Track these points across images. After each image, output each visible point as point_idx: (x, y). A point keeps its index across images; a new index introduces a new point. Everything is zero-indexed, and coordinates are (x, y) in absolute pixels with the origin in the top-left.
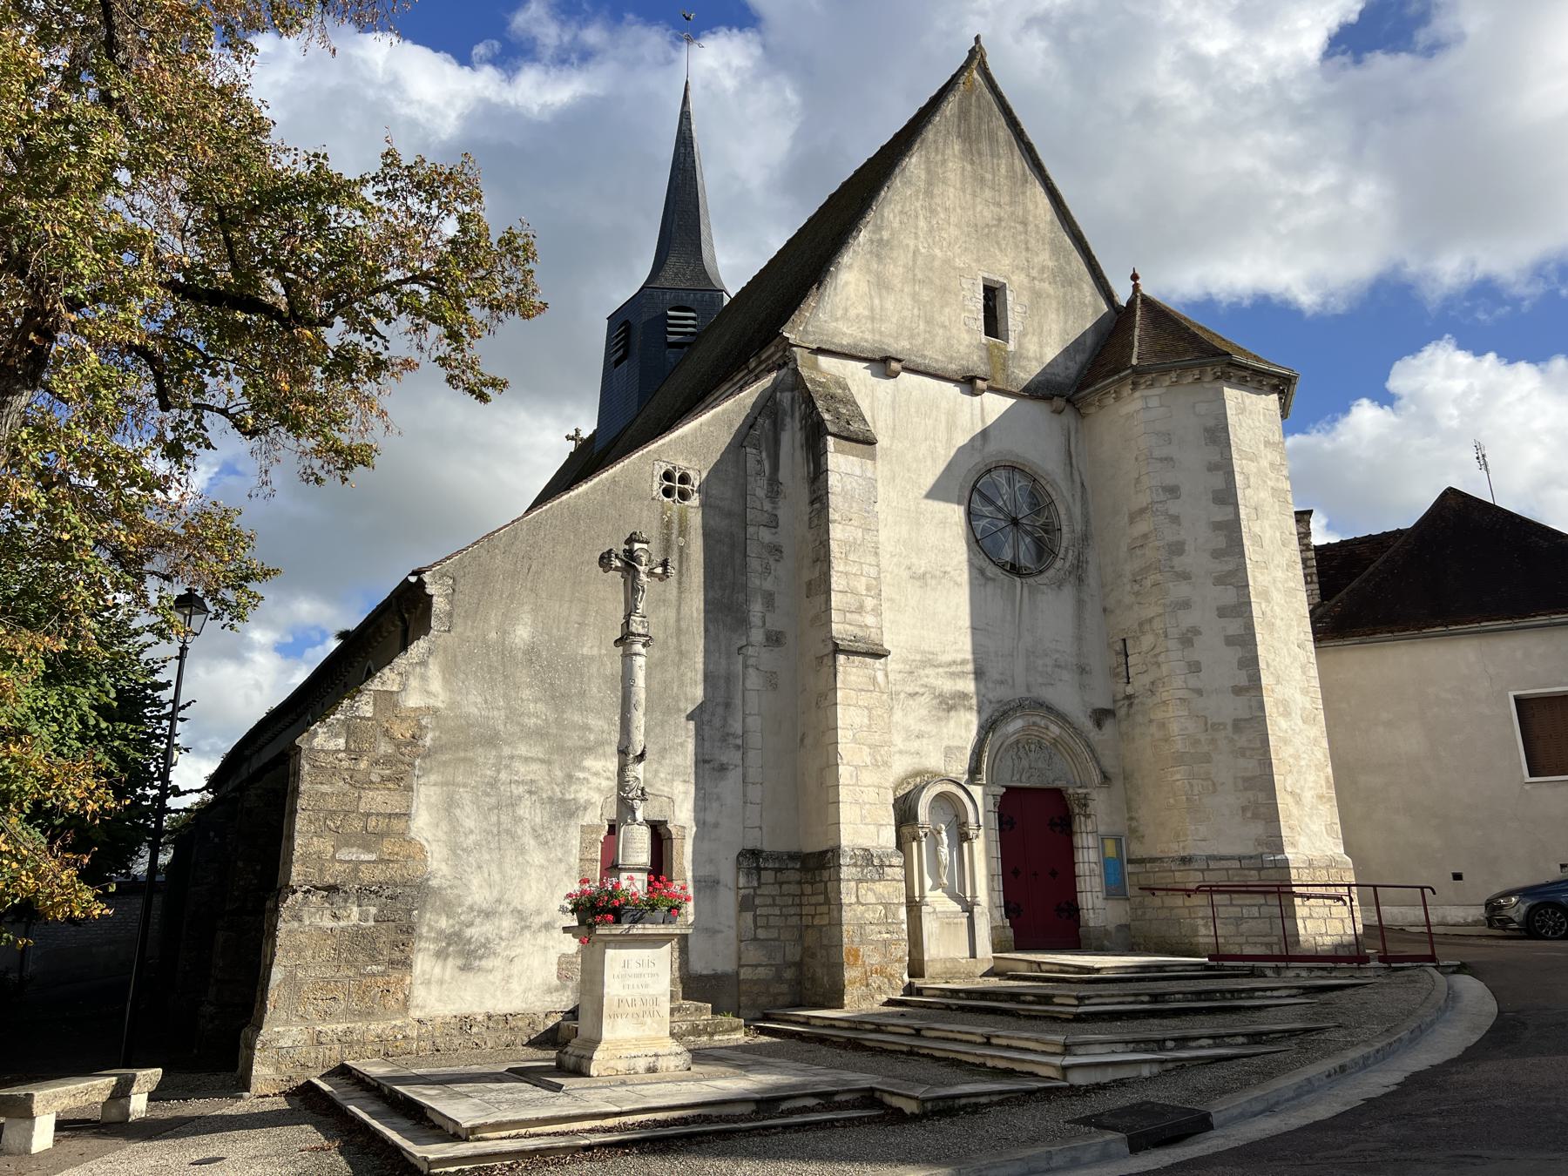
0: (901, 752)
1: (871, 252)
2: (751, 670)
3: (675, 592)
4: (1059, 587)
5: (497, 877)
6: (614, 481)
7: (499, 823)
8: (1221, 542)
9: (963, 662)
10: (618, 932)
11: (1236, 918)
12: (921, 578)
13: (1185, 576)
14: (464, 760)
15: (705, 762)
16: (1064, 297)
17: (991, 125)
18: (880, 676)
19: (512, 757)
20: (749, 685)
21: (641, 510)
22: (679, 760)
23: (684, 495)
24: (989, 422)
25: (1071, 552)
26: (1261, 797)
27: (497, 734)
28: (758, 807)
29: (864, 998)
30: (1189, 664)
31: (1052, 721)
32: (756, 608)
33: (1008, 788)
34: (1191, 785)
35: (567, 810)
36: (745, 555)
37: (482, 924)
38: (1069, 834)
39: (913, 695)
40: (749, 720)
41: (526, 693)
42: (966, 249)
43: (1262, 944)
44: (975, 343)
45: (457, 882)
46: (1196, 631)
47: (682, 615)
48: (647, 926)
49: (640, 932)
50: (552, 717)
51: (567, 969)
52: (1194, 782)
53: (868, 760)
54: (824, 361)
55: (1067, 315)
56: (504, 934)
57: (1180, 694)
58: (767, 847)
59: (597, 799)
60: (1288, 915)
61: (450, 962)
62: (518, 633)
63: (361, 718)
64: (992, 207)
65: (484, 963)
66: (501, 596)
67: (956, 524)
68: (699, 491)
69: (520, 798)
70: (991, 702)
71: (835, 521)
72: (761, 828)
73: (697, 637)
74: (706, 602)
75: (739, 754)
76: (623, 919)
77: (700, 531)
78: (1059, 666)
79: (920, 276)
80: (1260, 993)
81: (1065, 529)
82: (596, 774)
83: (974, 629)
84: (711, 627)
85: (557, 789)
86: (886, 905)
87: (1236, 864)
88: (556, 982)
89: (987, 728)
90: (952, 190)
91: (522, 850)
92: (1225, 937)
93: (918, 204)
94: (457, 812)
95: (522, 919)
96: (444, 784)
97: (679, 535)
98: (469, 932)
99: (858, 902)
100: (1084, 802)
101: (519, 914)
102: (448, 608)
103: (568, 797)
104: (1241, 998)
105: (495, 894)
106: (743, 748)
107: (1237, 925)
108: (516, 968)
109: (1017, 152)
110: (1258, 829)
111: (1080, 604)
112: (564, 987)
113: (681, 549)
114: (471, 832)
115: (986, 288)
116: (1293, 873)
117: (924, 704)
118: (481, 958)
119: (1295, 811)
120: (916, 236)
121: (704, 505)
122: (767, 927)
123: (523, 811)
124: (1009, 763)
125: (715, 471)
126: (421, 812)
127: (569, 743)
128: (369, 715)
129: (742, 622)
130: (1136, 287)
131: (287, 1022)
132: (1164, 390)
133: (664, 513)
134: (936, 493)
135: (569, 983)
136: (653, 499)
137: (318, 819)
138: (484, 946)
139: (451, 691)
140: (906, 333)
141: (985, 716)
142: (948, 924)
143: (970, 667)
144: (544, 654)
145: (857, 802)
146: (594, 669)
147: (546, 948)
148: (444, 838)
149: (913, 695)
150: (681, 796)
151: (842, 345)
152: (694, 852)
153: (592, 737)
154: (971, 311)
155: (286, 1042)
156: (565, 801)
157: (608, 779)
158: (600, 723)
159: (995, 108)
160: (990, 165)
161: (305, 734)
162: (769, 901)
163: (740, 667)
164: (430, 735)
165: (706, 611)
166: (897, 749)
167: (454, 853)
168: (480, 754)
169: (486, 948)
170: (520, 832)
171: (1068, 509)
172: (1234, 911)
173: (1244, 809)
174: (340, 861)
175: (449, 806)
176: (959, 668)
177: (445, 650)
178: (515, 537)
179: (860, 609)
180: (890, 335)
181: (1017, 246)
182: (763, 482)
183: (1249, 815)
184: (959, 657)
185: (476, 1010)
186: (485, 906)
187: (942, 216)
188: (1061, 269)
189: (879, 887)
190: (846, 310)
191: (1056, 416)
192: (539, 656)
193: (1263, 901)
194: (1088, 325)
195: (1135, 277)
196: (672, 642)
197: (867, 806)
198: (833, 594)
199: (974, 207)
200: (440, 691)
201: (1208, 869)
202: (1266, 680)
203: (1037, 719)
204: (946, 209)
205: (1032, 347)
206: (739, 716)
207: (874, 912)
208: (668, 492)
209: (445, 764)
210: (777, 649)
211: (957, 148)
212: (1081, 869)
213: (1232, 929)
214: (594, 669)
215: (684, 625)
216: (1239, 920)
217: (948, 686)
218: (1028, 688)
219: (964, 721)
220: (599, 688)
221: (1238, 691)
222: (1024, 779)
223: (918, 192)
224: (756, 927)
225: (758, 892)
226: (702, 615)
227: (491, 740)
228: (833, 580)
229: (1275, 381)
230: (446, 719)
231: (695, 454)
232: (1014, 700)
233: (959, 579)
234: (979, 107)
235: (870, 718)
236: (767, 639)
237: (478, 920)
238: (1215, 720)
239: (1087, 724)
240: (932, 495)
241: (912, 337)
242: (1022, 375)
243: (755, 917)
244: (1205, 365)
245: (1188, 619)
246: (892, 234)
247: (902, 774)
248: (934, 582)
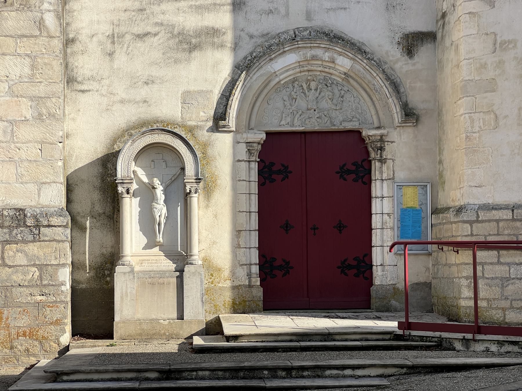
0: (122, 102)
11: (502, 279)
31: (340, 54)
33: (268, 134)
34: (472, 121)
39: (142, 37)
52: (476, 116)
53: (28, 114)
70: (251, 37)
80: (335, 372)
86: (41, 267)
87: (507, 215)
92: (488, 300)
104: (303, 377)
107: (503, 287)
124: (280, 104)
145: (11, 160)
149: (142, 37)
189: (33, 249)
197: (26, 164)
201: (477, 221)
203: (319, 52)
207: (25, 274)
212: (376, 221)
213: (496, 291)
216: (505, 281)
232: (286, 32)
235: (33, 67)
238: (506, 37)
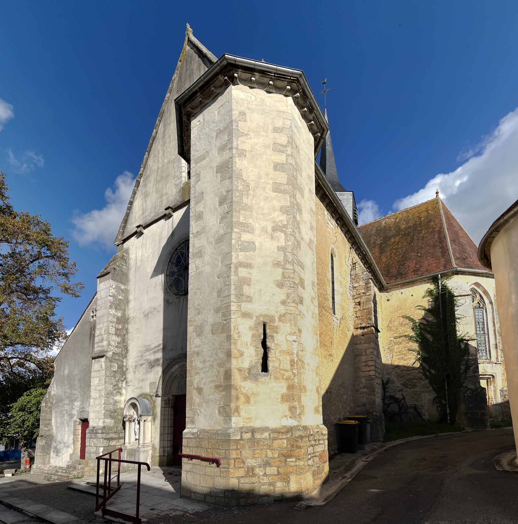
39: (141, 365)
89: (165, 372)
91: (65, 427)
143: (161, 347)
149: (141, 365)
207: (93, 449)
217: (152, 357)
240: (153, 276)
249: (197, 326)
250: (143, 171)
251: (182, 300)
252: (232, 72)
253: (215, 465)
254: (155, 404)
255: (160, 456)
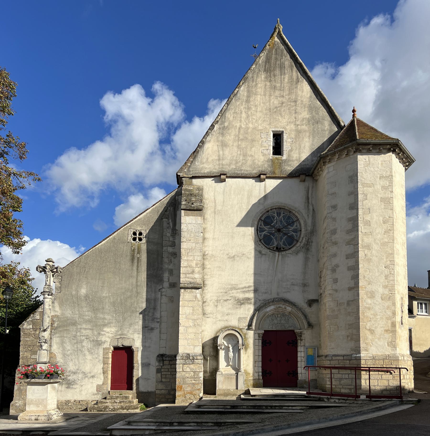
0: (220, 320)
1: (219, 133)
2: (163, 297)
3: (136, 273)
4: (297, 254)
5: (77, 363)
6: (114, 238)
7: (77, 348)
8: (350, 226)
9: (249, 287)
10: (27, 381)
12: (233, 258)
13: (335, 243)
14: (66, 330)
15: (145, 327)
16: (313, 130)
17: (282, 60)
18: (199, 296)
19: (81, 329)
20: (162, 301)
21: (124, 247)
22: (136, 327)
23: (140, 240)
24: (268, 191)
25: (304, 239)
26: (355, 332)
27: (76, 322)
28: (165, 341)
29: (183, 401)
30: (334, 280)
31: (288, 306)
32: (166, 275)
33: (265, 331)
34: (330, 328)
35: (98, 343)
36: (162, 257)
37: (73, 376)
38: (296, 347)
39: (226, 300)
40: (162, 313)
41: (85, 309)
42: (264, 121)
43: (348, 388)
44: (266, 159)
45: (65, 364)
46: (337, 266)
47: (138, 280)
48: (36, 379)
49: (34, 381)
50: (93, 316)
51: (99, 389)
52: (331, 326)
54: (195, 181)
55: (314, 137)
56: (79, 378)
57: (330, 292)
58: (168, 353)
59: (109, 340)
60: (358, 378)
61: (64, 386)
62: (82, 291)
63: (36, 319)
64: (279, 98)
65: (73, 386)
66: (76, 280)
67: (250, 235)
68: (145, 237)
69: (83, 340)
70: (260, 300)
71: (183, 242)
72: (166, 347)
73: (144, 287)
74: (147, 275)
75: (158, 324)
76: (29, 378)
77: (146, 251)
78: (293, 285)
79: (241, 137)
81: (303, 230)
82: (108, 332)
83: (255, 274)
84: (149, 284)
85: (95, 337)
86: (194, 372)
87: (341, 358)
88: (96, 392)
89: (257, 310)
90: (259, 96)
91: (85, 355)
92: (335, 385)
93: (242, 107)
94: (65, 345)
95: (85, 375)
96: (60, 337)
97: (138, 253)
98: (69, 378)
99: (183, 371)
100: (301, 334)
101: (84, 373)
102: (60, 285)
103: (98, 339)
104: (276, 409)
105: (77, 367)
106: (160, 322)
107: (340, 381)
108: (83, 388)
109: (295, 69)
110: (352, 344)
111: (306, 259)
112: (98, 394)
113: (138, 258)
114: (69, 350)
115: (274, 135)
116: (363, 362)
117: (230, 304)
118: (73, 385)
119: (370, 337)
120: (241, 121)
121: (147, 242)
122: (165, 378)
123: (84, 344)
125: (152, 230)
126: (54, 345)
127: (99, 324)
128: (38, 318)
129: (160, 280)
130: (354, 116)
131: (19, 400)
132: (335, 163)
133: (132, 247)
134: (243, 223)
135: (100, 393)
136: (128, 242)
137: (26, 348)
138: (74, 382)
139: (62, 310)
140: (234, 162)
141: (257, 306)
142: (228, 378)
143: (252, 288)
144: (91, 297)
145: (186, 339)
146: (107, 300)
147: (92, 383)
148: (61, 352)
149: (226, 300)
150: (137, 338)
151: (204, 173)
152: (142, 355)
153: (106, 321)
154: (265, 147)
155: (17, 405)
156: (98, 341)
157: (112, 334)
158: (109, 317)
159: (285, 52)
160: (279, 79)
161: (21, 325)
162: (167, 370)
163: (159, 296)
164: (56, 323)
165: (147, 278)
166: (218, 319)
167: (64, 356)
168: (71, 328)
169: (74, 382)
170: (84, 350)
171: (305, 222)
172: (339, 376)
173: (348, 336)
174: (33, 359)
175: (62, 343)
176: (247, 289)
177: (59, 298)
178: (80, 262)
179: (193, 272)
180: (227, 165)
181: (290, 113)
182: (170, 231)
183: (349, 338)
184: (247, 285)
185: (72, 399)
186: (74, 371)
187: (253, 109)
188: (313, 117)
189: (192, 366)
190: (208, 159)
191: (302, 183)
192: (89, 298)
193: (350, 372)
194: (326, 139)
195: (354, 111)
196: (135, 290)
198: (181, 268)
199: (270, 101)
200: (59, 310)
201: (332, 360)
202: (361, 283)
203: (281, 305)
204: (256, 106)
205: (295, 156)
206: (159, 312)
208: (134, 239)
209: (61, 331)
210: (173, 289)
211: (263, 76)
214: (107, 300)
215: (139, 284)
216: (341, 379)
217: (241, 296)
218: (278, 294)
219: (247, 308)
220: (109, 307)
221: (350, 289)
222: (274, 327)
223: (242, 102)
224: (162, 378)
225: (163, 367)
226: (146, 279)
227: (74, 324)
228: (181, 263)
229: (388, 147)
230: (61, 318)
231: (144, 224)
232: (271, 299)
233: (249, 256)
234: (276, 54)
235: (193, 310)
236: (170, 286)
237: (71, 375)
239: (305, 306)
240: (240, 225)
241: (237, 163)
242: (289, 168)
243: (161, 375)
244: (348, 147)
245: (335, 261)
246: (229, 123)
247: (220, 328)
248: (238, 258)
249: (367, 292)
250: (219, 119)
251: (277, 255)
252: (396, 148)
253: (389, 373)
254: (247, 336)
255: (254, 380)
